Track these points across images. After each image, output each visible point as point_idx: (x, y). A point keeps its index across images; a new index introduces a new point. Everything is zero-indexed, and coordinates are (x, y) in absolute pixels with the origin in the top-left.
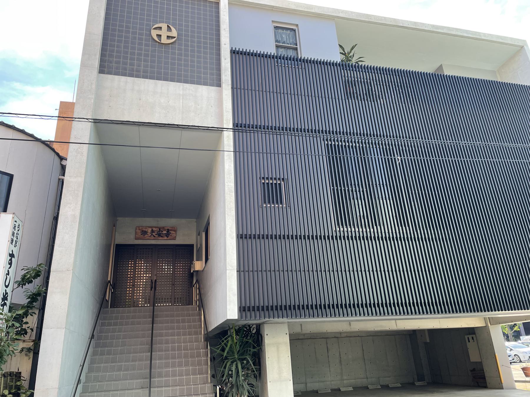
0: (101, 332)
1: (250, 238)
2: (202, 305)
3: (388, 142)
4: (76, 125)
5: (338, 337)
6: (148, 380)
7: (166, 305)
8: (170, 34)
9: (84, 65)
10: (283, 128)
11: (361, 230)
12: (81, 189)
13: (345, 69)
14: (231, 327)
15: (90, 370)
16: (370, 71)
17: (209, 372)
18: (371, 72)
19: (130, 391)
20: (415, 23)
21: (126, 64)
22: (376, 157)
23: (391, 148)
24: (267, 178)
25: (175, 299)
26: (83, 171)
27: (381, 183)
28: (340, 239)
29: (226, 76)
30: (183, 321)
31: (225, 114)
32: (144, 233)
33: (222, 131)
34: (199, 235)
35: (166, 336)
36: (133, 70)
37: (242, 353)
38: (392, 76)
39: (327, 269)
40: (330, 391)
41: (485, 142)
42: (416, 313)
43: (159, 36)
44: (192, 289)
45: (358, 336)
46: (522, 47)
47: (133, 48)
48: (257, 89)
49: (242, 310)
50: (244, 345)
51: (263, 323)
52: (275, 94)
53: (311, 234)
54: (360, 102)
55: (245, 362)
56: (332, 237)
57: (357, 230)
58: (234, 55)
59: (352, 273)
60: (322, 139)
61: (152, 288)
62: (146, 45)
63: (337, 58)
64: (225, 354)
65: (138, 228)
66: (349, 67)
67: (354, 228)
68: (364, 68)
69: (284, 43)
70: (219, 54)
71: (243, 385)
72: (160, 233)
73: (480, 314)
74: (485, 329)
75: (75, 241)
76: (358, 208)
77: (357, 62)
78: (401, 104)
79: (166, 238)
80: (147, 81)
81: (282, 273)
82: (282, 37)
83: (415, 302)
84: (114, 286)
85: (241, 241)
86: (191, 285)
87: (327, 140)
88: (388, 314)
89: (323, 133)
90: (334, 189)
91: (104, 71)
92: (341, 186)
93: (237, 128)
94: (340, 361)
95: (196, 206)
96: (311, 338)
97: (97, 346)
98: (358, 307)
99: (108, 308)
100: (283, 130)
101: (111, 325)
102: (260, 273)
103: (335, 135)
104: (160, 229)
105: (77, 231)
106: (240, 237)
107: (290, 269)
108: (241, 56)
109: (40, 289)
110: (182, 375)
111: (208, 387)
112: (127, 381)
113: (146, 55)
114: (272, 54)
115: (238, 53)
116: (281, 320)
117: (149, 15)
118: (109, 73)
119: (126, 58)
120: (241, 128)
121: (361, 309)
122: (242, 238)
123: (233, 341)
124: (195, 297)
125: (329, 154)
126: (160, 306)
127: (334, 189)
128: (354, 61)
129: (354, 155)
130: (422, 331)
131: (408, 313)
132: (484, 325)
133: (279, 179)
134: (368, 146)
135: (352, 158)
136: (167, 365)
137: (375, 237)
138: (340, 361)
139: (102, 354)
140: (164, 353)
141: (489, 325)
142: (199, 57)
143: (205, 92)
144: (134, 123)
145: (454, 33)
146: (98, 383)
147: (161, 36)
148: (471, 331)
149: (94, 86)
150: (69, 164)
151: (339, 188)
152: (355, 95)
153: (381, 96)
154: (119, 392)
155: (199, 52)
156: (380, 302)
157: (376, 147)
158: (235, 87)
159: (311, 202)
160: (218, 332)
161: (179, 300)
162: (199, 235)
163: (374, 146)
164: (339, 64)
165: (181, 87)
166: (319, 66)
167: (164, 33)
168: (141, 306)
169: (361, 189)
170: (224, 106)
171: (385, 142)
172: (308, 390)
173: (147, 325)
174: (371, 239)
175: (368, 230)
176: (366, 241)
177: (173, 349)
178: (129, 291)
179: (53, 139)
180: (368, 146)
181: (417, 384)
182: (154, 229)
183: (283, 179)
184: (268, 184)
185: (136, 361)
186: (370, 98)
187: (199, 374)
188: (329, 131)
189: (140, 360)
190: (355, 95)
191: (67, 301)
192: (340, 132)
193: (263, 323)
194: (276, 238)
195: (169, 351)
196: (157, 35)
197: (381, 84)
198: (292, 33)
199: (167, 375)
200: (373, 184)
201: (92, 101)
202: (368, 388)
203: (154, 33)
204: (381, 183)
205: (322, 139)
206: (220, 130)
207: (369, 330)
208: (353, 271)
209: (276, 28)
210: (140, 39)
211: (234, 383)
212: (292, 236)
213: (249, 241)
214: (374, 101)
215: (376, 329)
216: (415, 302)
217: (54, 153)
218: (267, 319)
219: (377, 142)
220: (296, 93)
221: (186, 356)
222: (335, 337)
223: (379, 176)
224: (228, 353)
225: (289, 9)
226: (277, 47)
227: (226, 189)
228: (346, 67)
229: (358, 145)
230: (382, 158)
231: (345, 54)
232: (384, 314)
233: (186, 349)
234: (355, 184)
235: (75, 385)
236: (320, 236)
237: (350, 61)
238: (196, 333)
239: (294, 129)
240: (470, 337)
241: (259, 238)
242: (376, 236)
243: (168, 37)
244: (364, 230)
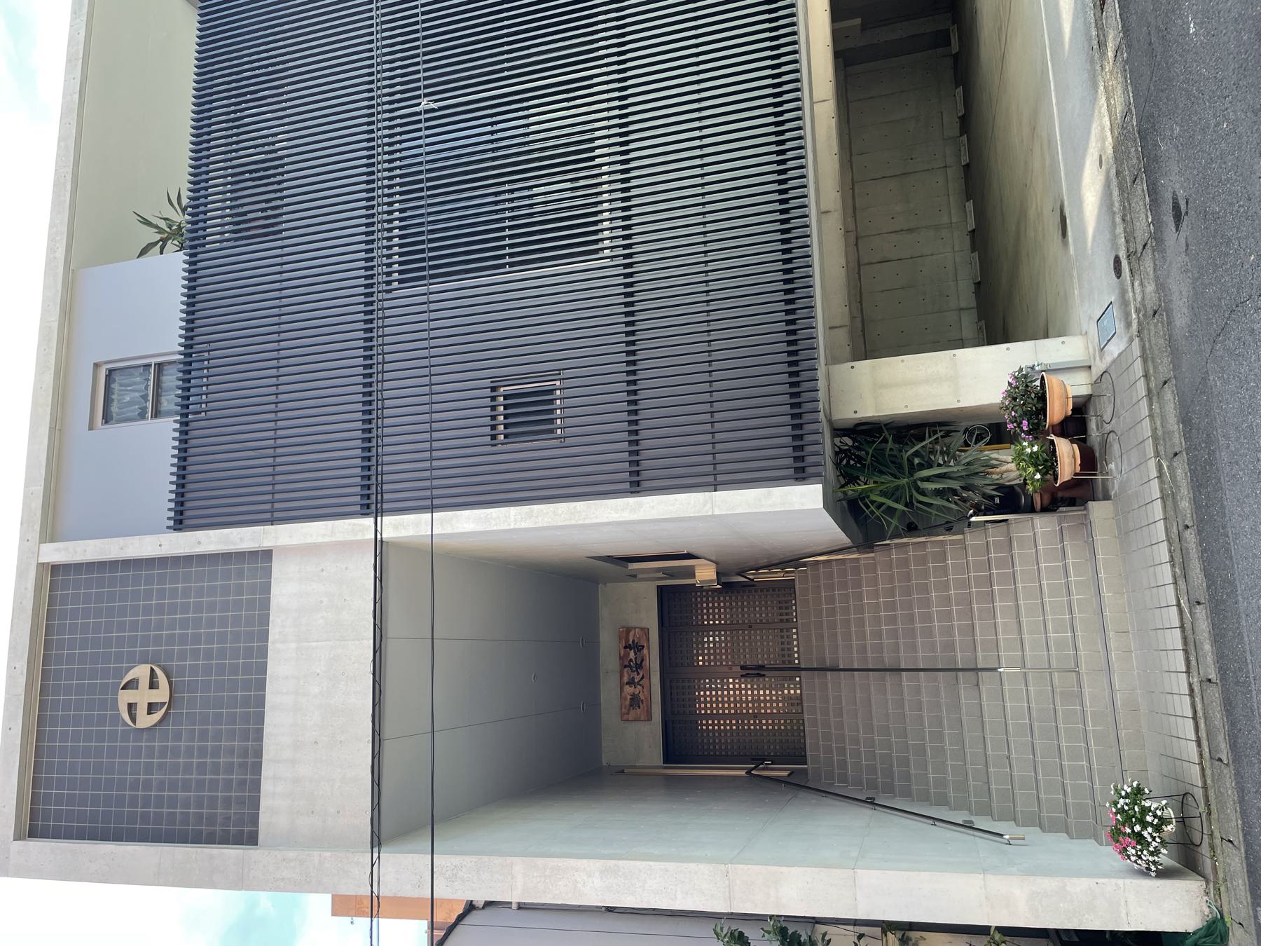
0: (859, 782)
1: (637, 453)
2: (794, 561)
3: (385, 128)
4: (387, 889)
5: (855, 238)
6: (960, 674)
7: (797, 640)
8: (144, 682)
9: (239, 883)
10: (365, 367)
11: (606, 196)
12: (540, 861)
13: (202, 241)
14: (840, 495)
15: (943, 801)
16: (204, 177)
17: (941, 538)
18: (209, 133)
19: (985, 709)
21: (228, 783)
22: (422, 147)
23: (399, 121)
24: (494, 408)
25: (781, 621)
26: (497, 861)
27: (489, 137)
30: (831, 600)
31: (339, 537)
32: (635, 701)
33: (382, 541)
34: (635, 576)
35: (864, 638)
36: (243, 766)
37: (897, 468)
38: (214, 120)
40: (976, 254)
42: (796, 61)
43: (152, 708)
44: (759, 585)
45: (853, 189)
47: (188, 768)
48: (270, 461)
49: (802, 475)
50: (882, 464)
51: (830, 422)
52: (280, 415)
53: (622, 290)
54: (286, 201)
55: (917, 461)
56: (626, 266)
57: (606, 196)
58: (187, 522)
59: (708, 198)
60: (387, 296)
61: (759, 675)
62: (178, 736)
63: (174, 262)
64: (900, 507)
65: (625, 717)
66: (196, 231)
67: (602, 212)
68: (198, 190)
69: (145, 397)
70: (188, 560)
71: (968, 464)
72: (633, 665)
75: (662, 865)
76: (552, 192)
77: (184, 210)
78: (285, 97)
79: (645, 651)
80: (268, 729)
81: (715, 345)
82: (132, 403)
84: (758, 760)
85: (645, 485)
86: (750, 586)
87: (390, 230)
88: (798, 109)
89: (372, 250)
90: (511, 265)
92: (503, 238)
93: (373, 507)
94: (910, 230)
95: (566, 591)
96: (861, 302)
97: (889, 789)
98: (785, 191)
100: (370, 385)
101: (845, 762)
102: (717, 416)
103: (375, 263)
104: (625, 665)
105: (638, 863)
106: (636, 485)
107: (705, 367)
108: (188, 505)
109: (770, 929)
110: (948, 598)
111: (972, 539)
112: (964, 718)
113: (204, 735)
114: (178, 426)
115: (182, 513)
116: (821, 384)
117: (100, 737)
120: (374, 497)
121: (791, 174)
122: (638, 483)
123: (871, 490)
124: (777, 575)
125: (423, 278)
126: (798, 652)
127: (511, 265)
128: (179, 218)
129: (421, 146)
131: (795, 43)
133: (493, 398)
134: (398, 163)
136: (928, 632)
137: (622, 144)
138: (910, 230)
139: (907, 777)
140: (901, 641)
142: (198, 608)
143: (287, 588)
144: (376, 755)
146: (971, 782)
147: (150, 705)
149: (291, 854)
150: (480, 898)
151: (507, 232)
152: (270, 213)
153: (266, 148)
154: (988, 736)
155: (185, 608)
156: (771, 110)
157: (400, 142)
158: (268, 516)
159: (548, 307)
160: (852, 521)
161: (784, 611)
162: (635, 576)
163: (398, 155)
164: (191, 255)
165: (278, 645)
166: (198, 306)
167: (143, 696)
168: (800, 689)
169: (507, 196)
170: (320, 540)
171: (385, 136)
172: (974, 304)
173: (843, 682)
174: (625, 79)
175: (605, 178)
176: (632, 155)
177: (892, 620)
178: (767, 724)
179: (424, 924)
180: (398, 163)
181: (955, 47)
182: (626, 679)
183: (494, 389)
184: (506, 407)
185: (920, 703)
186: (274, 175)
187: (945, 560)
188: (367, 269)
189: (918, 691)
190: (270, 213)
191: (795, 871)
192: (367, 251)
193: (830, 422)
194: (635, 402)
195: (896, 630)
196: (149, 713)
197: (235, 139)
198: (117, 377)
199: (949, 631)
200: (493, 150)
201: (328, 854)
202: (967, 166)
203: (145, 721)
204: (489, 137)
205: (387, 296)
206: (380, 547)
207: (837, 166)
209: (107, 419)
210: (163, 753)
211: (962, 483)
212: (629, 363)
213: (644, 454)
214: (282, 166)
215: (835, 149)
216: (768, 44)
217: (459, 929)
218: (821, 416)
219: (386, 157)
220: (275, 337)
221: (907, 591)
222: (856, 245)
223: (470, 137)
224: (897, 501)
225: (52, 429)
226: (157, 414)
227: (524, 525)
228: (198, 238)
229: (398, 180)
230: (427, 136)
231: (164, 241)
232: (800, 138)
233: (891, 592)
234: (496, 203)
235: (976, 833)
236: (627, 304)
237: (180, 228)
238: (856, 570)
239: (365, 367)
241: (636, 432)
242: (618, 139)
243: (153, 685)
244: (605, 178)
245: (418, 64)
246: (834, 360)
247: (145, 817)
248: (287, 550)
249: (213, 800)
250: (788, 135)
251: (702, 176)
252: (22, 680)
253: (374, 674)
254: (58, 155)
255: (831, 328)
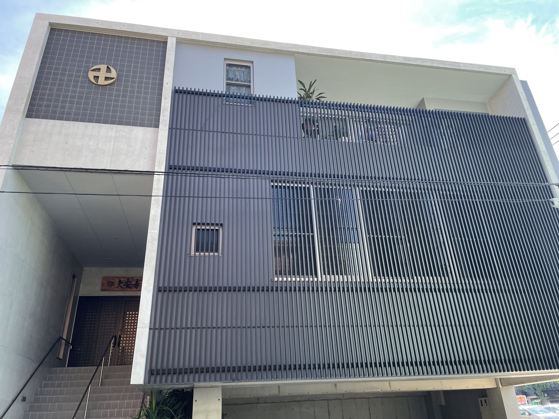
5: (354, 398)
9: (9, 110)
20: (385, 56)
28: (411, 291)
29: (164, 116)
31: (158, 155)
36: (63, 113)
39: (403, 324)
41: (522, 182)
43: (96, 78)
46: (510, 76)
59: (425, 328)
63: (293, 94)
68: (403, 111)
69: (237, 80)
70: (160, 94)
73: (490, 374)
74: (496, 390)
77: (318, 99)
79: (135, 289)
80: (77, 123)
82: (235, 75)
83: (499, 358)
87: (395, 188)
91: (32, 115)
92: (381, 234)
96: (309, 400)
99: (65, 366)
118: (37, 117)
119: (57, 101)
121: (402, 368)
125: (363, 198)
128: (314, 98)
130: (437, 393)
132: (495, 386)
135: (433, 202)
141: (500, 386)
142: (138, 97)
143: (140, 134)
144: (62, 169)
145: (418, 63)
147: (98, 77)
148: (483, 393)
149: (15, 131)
156: (457, 359)
165: (115, 129)
170: (158, 148)
180: (423, 192)
182: (122, 280)
196: (94, 77)
200: (396, 229)
203: (91, 75)
206: (152, 173)
208: (414, 326)
209: (229, 65)
225: (226, 44)
231: (305, 91)
240: (483, 399)
243: (107, 78)
245: (412, 198)
246: (224, 389)
247: (49, 73)
248: (157, 133)
249: (50, 100)
250: (446, 367)
251: (451, 325)
252: (118, 28)
253: (74, 168)
254: (287, 44)
255: (279, 387)
